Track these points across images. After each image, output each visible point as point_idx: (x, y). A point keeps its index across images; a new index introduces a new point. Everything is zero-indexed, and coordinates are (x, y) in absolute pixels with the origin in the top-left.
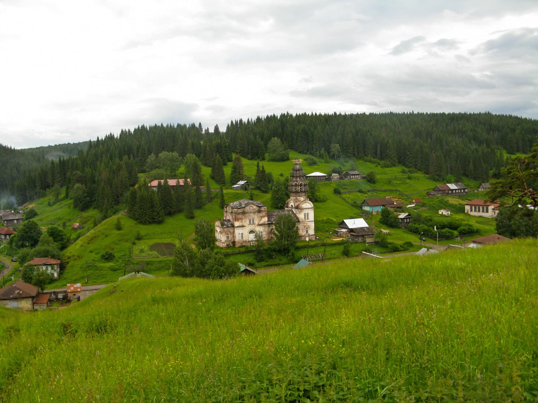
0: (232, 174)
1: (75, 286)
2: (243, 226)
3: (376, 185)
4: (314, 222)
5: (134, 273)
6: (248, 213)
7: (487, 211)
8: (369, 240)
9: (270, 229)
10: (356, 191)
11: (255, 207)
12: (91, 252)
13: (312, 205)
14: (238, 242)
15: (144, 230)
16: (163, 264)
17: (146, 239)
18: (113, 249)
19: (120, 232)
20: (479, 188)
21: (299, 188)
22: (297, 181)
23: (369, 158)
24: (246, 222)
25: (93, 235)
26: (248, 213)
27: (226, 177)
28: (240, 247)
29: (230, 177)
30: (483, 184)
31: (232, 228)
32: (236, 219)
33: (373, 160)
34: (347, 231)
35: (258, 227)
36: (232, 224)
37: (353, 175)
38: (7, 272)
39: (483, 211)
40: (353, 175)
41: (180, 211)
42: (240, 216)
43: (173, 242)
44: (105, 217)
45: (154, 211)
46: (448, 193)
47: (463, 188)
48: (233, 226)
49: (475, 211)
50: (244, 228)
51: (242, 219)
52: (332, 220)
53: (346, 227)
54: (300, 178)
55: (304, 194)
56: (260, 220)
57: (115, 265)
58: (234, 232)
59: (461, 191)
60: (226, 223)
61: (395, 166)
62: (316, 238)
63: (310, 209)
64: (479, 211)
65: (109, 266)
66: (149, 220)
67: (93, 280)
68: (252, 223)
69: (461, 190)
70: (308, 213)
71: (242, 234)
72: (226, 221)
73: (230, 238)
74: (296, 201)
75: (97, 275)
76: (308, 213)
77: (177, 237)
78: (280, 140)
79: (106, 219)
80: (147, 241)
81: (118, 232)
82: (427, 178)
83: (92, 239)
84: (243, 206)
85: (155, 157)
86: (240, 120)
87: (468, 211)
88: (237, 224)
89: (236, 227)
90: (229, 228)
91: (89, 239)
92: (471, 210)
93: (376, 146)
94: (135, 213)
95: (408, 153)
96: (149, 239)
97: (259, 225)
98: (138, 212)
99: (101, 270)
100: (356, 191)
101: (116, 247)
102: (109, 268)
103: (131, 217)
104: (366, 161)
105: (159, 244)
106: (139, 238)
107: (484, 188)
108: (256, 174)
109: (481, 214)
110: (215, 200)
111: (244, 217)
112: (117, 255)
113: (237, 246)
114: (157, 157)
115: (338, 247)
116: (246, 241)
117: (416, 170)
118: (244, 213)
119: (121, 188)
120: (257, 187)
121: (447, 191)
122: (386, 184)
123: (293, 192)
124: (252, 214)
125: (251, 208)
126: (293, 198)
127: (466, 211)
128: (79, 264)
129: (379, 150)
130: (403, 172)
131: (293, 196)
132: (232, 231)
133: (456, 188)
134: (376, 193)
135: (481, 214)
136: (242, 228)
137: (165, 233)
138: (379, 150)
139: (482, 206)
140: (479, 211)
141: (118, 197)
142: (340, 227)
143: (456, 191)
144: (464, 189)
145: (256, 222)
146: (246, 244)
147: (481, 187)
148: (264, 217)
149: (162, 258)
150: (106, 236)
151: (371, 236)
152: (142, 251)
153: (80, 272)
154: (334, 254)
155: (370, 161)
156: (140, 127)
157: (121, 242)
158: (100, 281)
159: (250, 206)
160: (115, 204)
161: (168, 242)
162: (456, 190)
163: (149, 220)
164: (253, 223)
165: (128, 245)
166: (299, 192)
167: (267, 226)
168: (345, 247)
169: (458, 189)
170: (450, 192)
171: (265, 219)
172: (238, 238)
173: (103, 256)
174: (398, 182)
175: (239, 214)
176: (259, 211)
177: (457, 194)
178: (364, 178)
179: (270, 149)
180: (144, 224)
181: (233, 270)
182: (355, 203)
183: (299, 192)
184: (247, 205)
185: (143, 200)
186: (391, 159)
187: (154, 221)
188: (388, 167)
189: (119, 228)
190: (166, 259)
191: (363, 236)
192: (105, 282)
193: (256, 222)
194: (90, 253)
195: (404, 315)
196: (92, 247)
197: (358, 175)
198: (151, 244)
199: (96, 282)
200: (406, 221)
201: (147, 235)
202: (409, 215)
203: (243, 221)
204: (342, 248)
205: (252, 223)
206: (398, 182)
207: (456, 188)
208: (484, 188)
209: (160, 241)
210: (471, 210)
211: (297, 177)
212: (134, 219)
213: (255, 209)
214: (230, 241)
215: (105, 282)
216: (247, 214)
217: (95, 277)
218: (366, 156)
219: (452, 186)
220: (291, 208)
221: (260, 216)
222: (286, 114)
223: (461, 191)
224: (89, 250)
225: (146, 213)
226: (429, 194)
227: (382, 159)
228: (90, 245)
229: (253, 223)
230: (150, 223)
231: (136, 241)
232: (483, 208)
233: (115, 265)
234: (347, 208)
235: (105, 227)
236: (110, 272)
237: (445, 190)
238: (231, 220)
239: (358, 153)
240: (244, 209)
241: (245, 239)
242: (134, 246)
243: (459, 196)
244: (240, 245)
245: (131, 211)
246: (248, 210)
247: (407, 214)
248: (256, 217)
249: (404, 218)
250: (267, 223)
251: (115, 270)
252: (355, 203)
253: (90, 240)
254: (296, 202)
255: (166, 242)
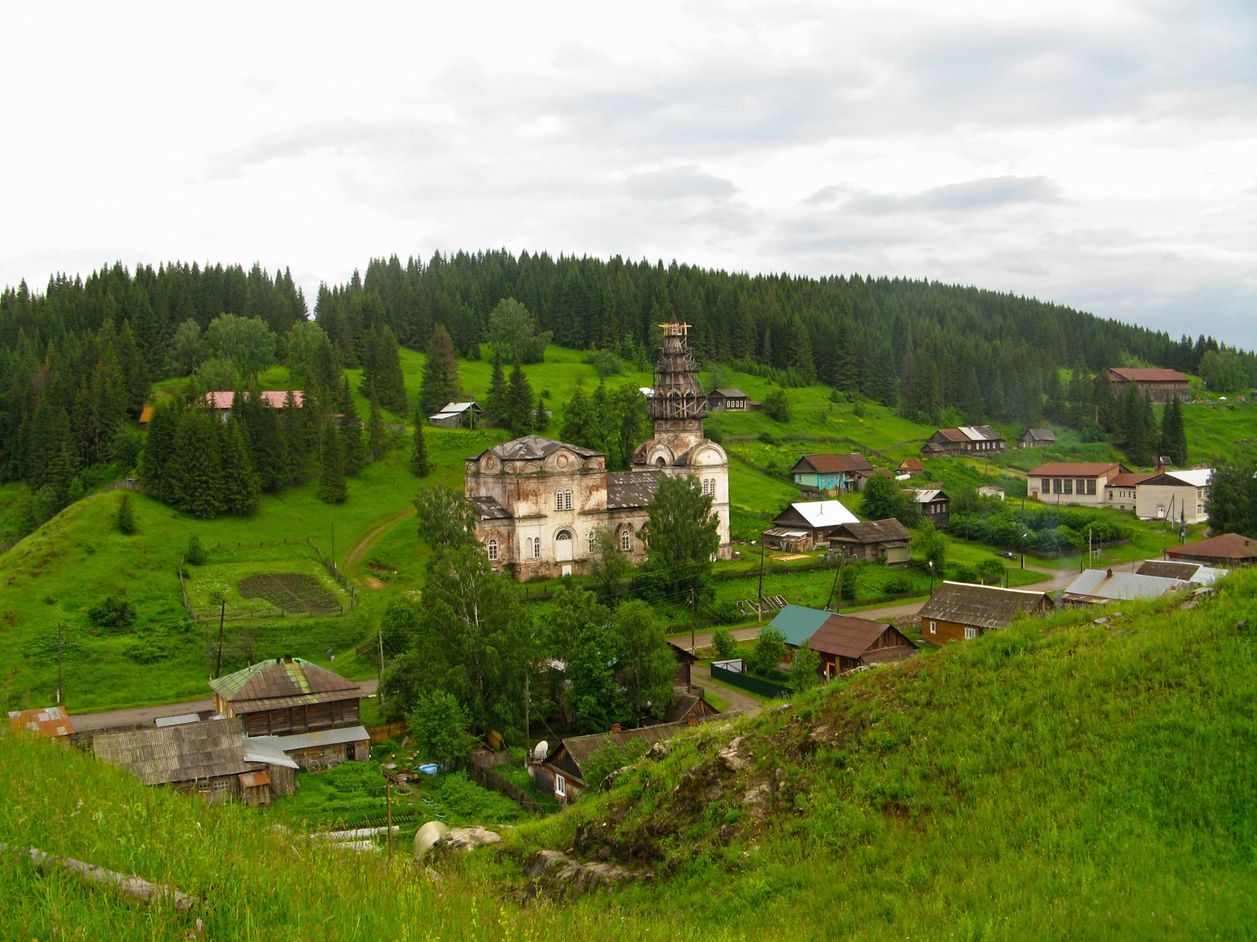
0: (425, 384)
1: (43, 717)
2: (539, 516)
3: (792, 427)
4: (727, 508)
5: (272, 662)
6: (552, 475)
7: (1092, 491)
8: (893, 556)
9: (614, 527)
10: (754, 440)
11: (572, 458)
12: (50, 602)
13: (725, 457)
14: (527, 566)
15: (210, 533)
16: (309, 638)
17: (219, 562)
18: (122, 592)
19: (135, 538)
20: (1021, 440)
21: (684, 408)
22: (678, 386)
23: (748, 361)
24: (548, 504)
25: (46, 549)
26: (552, 475)
27: (409, 395)
28: (531, 581)
29: (422, 393)
30: (1032, 431)
31: (506, 522)
32: (520, 495)
33: (756, 367)
34: (808, 535)
35: (583, 518)
36: (502, 510)
37: (731, 399)
38: (766, 426)
39: (1080, 492)
40: (731, 399)
41: (298, 483)
42: (532, 485)
43: (307, 572)
44: (62, 502)
45: (231, 476)
46: (966, 451)
47: (995, 438)
48: (509, 517)
49: (1058, 490)
50: (542, 521)
51: (536, 494)
52: (741, 509)
53: (803, 524)
54: (685, 377)
55: (696, 424)
56: (588, 498)
57: (143, 643)
58: (511, 535)
59: (991, 446)
60: (484, 507)
61: (809, 384)
62: (733, 555)
63: (719, 470)
64: (1069, 491)
65: (123, 650)
66: (217, 504)
67: (82, 697)
68: (564, 507)
69: (991, 442)
70: (713, 480)
71: (537, 539)
72: (483, 502)
73: (499, 553)
74: (672, 445)
75: (91, 678)
76: (713, 480)
77: (315, 556)
78: (522, 305)
79: (65, 506)
80: (223, 567)
81: (127, 539)
82: (896, 415)
83: (46, 562)
84: (540, 454)
85: (199, 328)
86: (391, 260)
87: (1035, 493)
88: (522, 508)
89: (519, 519)
90: (497, 523)
91: (35, 562)
92: (1046, 491)
93: (761, 336)
94: (173, 481)
95: (841, 353)
96: (228, 561)
97: (585, 513)
98: (180, 480)
99: (97, 661)
100: (754, 440)
101: (133, 585)
102: (124, 654)
103: (155, 498)
104: (741, 370)
105: (265, 577)
106: (195, 558)
107: (1034, 441)
108: (491, 386)
109: (1074, 498)
110: (394, 453)
111: (541, 488)
112: (143, 612)
113: (524, 575)
114: (205, 329)
115: (816, 576)
116: (548, 563)
117: (861, 395)
118: (542, 476)
119: (102, 415)
120: (502, 420)
121: (962, 446)
122: (813, 424)
123: (666, 420)
124: (565, 480)
125: (563, 460)
126: (664, 436)
127: (1030, 493)
128: (15, 644)
129: (767, 343)
130: (834, 399)
131: (667, 431)
132: (504, 530)
133: (980, 437)
134: (802, 445)
135: (1074, 498)
136: (535, 522)
137: (272, 545)
138: (767, 343)
139: (1076, 477)
140: (1069, 491)
141: (92, 442)
142: (777, 525)
143: (981, 447)
144: (998, 441)
145: (577, 505)
146: (547, 573)
147: (1027, 437)
148: (597, 488)
149: (292, 620)
150: (91, 552)
151: (898, 544)
152: (217, 598)
153: (27, 671)
154: (816, 597)
155: (751, 372)
156: (98, 274)
157: (145, 571)
158: (108, 698)
159: (559, 453)
160: (81, 463)
161: (289, 571)
162: (980, 442)
163: (217, 504)
164: (569, 509)
165: (167, 579)
166: (683, 419)
167: (606, 516)
168: (845, 574)
169: (985, 442)
170: (969, 447)
171: (601, 497)
172: (525, 554)
173: (95, 616)
174: (841, 421)
175: (529, 477)
176: (585, 472)
177: (984, 454)
178: (757, 408)
179: (496, 330)
180: (200, 518)
181: (652, 637)
182: (772, 465)
183: (683, 419)
184: (549, 450)
185: (198, 441)
186: (801, 366)
187: (230, 509)
188: (796, 386)
189: (126, 526)
190: (311, 622)
191: (876, 545)
192: (126, 700)
193: (577, 505)
194: (49, 607)
195: (1220, 771)
196: (47, 587)
197: (743, 399)
198: (240, 578)
199: (92, 703)
200: (933, 512)
201: (218, 549)
202: (941, 495)
203: (541, 500)
204: (830, 578)
205: (564, 507)
206: (841, 421)
207: (981, 438)
208: (1034, 441)
209: (264, 569)
210: (1046, 491)
211: (677, 374)
212: (165, 502)
213: (572, 465)
214: (499, 562)
215: (126, 700)
216: (552, 479)
217: (87, 687)
218: (736, 356)
219: (973, 434)
220: (656, 466)
221: (587, 487)
222: (500, 252)
223: (991, 446)
224: (40, 596)
225: (206, 482)
226: (928, 449)
227: (778, 364)
228: (39, 580)
229: (569, 509)
230: (220, 514)
231: (192, 570)
232: (1080, 485)
233: (143, 643)
234: (758, 480)
235: (80, 523)
236: (135, 667)
237: (958, 443)
238: (500, 500)
239: (717, 348)
240: (541, 463)
241: (545, 555)
242: (188, 585)
243: (989, 458)
244: (532, 575)
245: (156, 476)
246: (554, 468)
247: (936, 492)
248: (575, 488)
249: (931, 503)
250: (605, 507)
251: (147, 661)
252: (772, 465)
253: (39, 566)
254: (677, 447)
255: (282, 571)
